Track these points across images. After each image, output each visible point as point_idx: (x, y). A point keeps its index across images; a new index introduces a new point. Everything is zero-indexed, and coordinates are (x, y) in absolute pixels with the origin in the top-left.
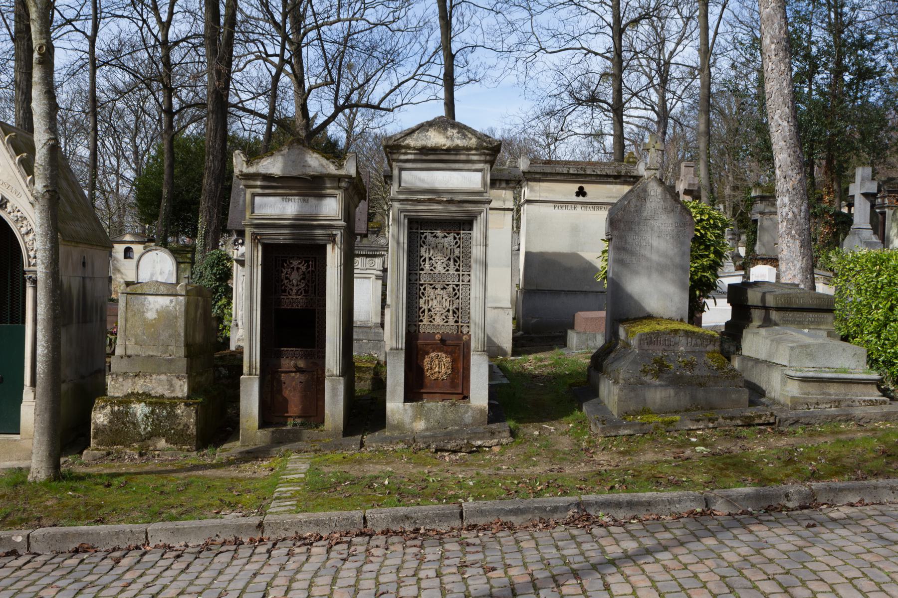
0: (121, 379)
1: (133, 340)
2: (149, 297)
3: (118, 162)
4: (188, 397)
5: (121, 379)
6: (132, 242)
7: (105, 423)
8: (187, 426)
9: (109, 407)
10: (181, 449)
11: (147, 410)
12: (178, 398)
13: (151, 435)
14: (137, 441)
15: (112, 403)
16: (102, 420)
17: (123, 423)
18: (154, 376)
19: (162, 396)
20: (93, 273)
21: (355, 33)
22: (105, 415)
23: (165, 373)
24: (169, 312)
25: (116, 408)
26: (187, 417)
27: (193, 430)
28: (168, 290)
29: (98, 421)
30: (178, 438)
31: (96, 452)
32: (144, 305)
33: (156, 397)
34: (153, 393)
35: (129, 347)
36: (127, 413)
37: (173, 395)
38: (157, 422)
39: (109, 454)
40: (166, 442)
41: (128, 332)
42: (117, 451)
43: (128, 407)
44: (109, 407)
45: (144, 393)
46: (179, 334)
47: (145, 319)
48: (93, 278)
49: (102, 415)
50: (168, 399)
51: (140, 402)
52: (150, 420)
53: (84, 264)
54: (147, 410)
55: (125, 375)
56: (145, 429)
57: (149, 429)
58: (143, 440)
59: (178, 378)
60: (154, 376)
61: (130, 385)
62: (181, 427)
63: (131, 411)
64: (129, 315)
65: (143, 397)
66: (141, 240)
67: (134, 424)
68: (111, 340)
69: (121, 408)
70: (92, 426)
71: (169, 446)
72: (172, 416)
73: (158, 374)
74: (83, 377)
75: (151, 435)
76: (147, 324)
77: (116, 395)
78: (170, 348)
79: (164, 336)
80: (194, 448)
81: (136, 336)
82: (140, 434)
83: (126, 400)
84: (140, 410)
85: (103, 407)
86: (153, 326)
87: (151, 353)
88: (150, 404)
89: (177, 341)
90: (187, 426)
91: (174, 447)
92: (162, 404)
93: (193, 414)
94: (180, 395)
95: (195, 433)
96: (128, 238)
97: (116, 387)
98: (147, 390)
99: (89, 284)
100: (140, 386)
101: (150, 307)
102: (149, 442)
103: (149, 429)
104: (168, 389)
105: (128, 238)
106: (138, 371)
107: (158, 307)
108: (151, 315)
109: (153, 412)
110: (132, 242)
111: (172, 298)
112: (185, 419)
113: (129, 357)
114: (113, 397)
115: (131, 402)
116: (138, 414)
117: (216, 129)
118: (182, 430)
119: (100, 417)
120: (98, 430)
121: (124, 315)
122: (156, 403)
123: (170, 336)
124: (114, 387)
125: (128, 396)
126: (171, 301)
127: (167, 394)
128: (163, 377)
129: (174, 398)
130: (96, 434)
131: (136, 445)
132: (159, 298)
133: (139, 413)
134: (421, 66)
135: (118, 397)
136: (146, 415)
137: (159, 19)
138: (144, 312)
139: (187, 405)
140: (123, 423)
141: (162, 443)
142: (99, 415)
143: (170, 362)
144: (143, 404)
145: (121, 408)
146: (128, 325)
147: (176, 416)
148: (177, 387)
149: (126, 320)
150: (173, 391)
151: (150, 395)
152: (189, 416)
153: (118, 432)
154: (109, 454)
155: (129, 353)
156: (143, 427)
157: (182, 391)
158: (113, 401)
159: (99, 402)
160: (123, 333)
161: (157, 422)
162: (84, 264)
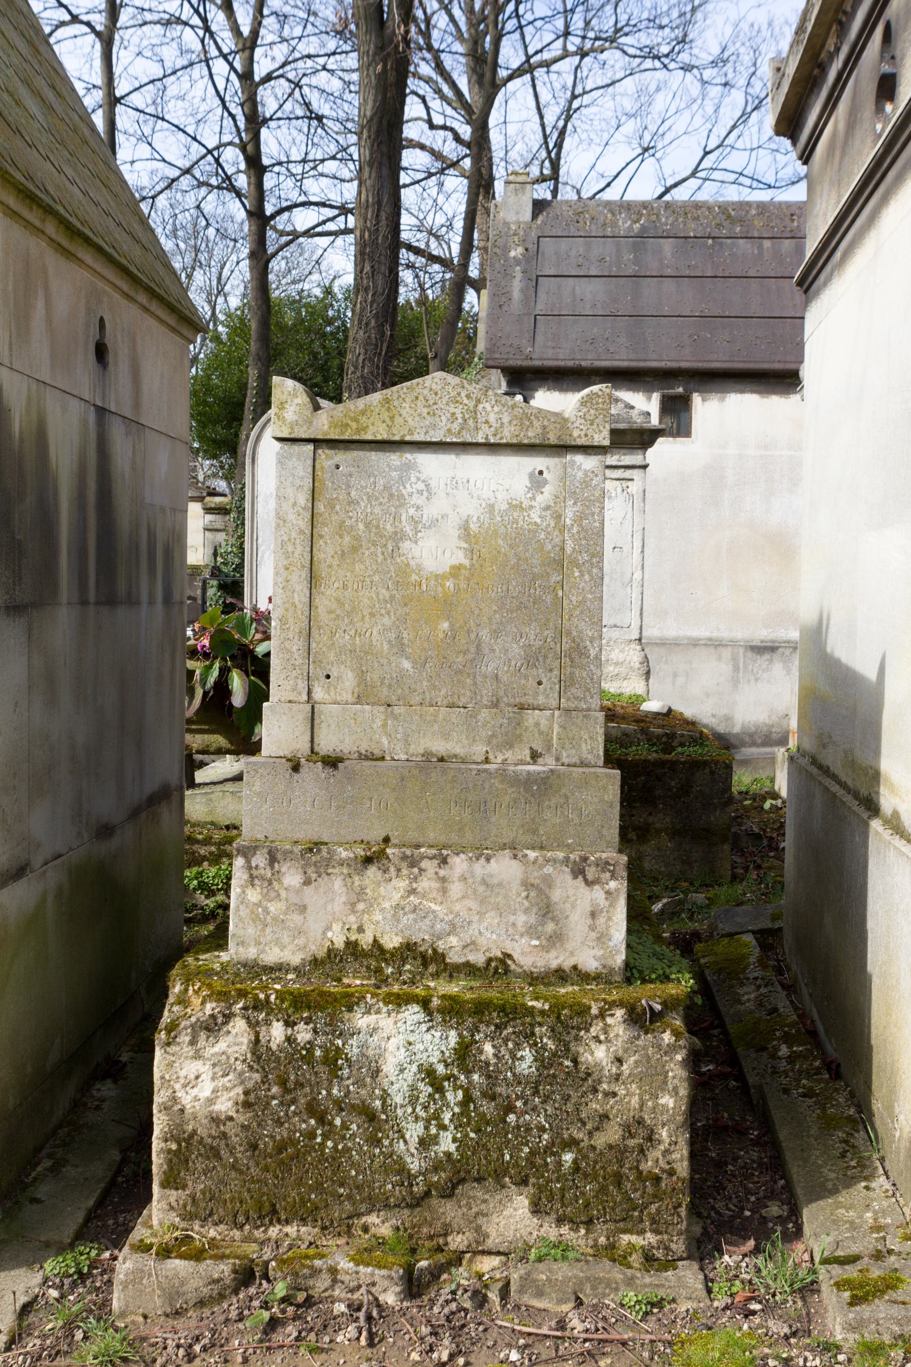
0: (292, 877)
1: (348, 680)
4: (632, 972)
5: (292, 877)
7: (224, 1106)
8: (641, 1130)
9: (239, 1025)
10: (611, 1252)
11: (437, 1044)
12: (580, 976)
13: (456, 1177)
14: (385, 1205)
15: (257, 1006)
16: (205, 1090)
17: (313, 1110)
18: (459, 864)
19: (499, 968)
20: (137, 404)
21: (585, 93)
22: (222, 1066)
23: (514, 848)
25: (277, 1032)
26: (639, 1077)
27: (671, 1152)
29: (186, 1099)
30: (596, 1194)
31: (176, 1264)
33: (469, 969)
34: (454, 948)
35: (328, 713)
36: (333, 1060)
37: (555, 959)
38: (487, 1108)
39: (247, 1275)
40: (536, 1209)
41: (320, 641)
42: (296, 1265)
43: (335, 1028)
44: (239, 1025)
45: (409, 949)
47: (405, 570)
48: (135, 425)
49: (202, 1068)
50: (533, 979)
51: (399, 1001)
52: (454, 1097)
53: (101, 352)
54: (437, 1044)
55: (313, 854)
56: (425, 1143)
57: (447, 1144)
58: (418, 1202)
59: (578, 871)
60: (459, 864)
61: (339, 904)
62: (612, 1134)
63: (353, 1048)
64: (327, 551)
65: (405, 969)
67: (371, 1116)
69: (303, 1034)
70: (160, 1124)
71: (551, 1231)
72: (561, 1075)
73: (481, 851)
74: (105, 831)
75: (456, 1177)
77: (272, 956)
78: (532, 717)
80: (679, 1246)
81: (361, 657)
82: (402, 1170)
83: (325, 989)
84: (398, 1043)
85: (212, 1028)
86: (447, 606)
87: (440, 747)
88: (451, 1011)
90: (641, 1130)
91: (577, 1238)
92: (511, 1012)
93: (676, 1071)
94: (590, 962)
95: (683, 1168)
97: (275, 921)
98: (421, 934)
99: (121, 446)
100: (388, 911)
101: (431, 511)
102: (449, 1211)
103: (447, 1144)
104: (531, 931)
106: (375, 834)
107: (471, 509)
108: (435, 553)
109: (464, 1054)
111: (538, 462)
112: (631, 1097)
113: (332, 762)
114: (256, 969)
115: (350, 1001)
116: (389, 1067)
117: (379, 203)
118: (618, 1151)
119: (197, 1078)
120: (186, 1146)
122: (480, 1009)
123: (532, 659)
124: (260, 919)
125: (331, 961)
126: (537, 480)
127: (528, 955)
128: (504, 868)
129: (561, 976)
130: (179, 1162)
131: (381, 1225)
132: (476, 466)
133: (393, 1059)
134: (706, 153)
135: (280, 968)
136: (429, 1073)
137: (236, 29)
138: (398, 537)
139: (642, 1020)
140: (313, 1110)
141: (513, 1216)
142: (191, 1068)
143: (539, 788)
144: (413, 1013)
145: (303, 1034)
146: (323, 603)
147: (585, 1079)
148: (577, 923)
150: (555, 940)
151: (439, 957)
152: (653, 1080)
153: (287, 1155)
154: (247, 1275)
155: (327, 743)
156: (414, 1131)
157: (602, 938)
158: (248, 991)
159: (186, 1000)
160: (297, 646)
161: (487, 1108)
162: (101, 352)
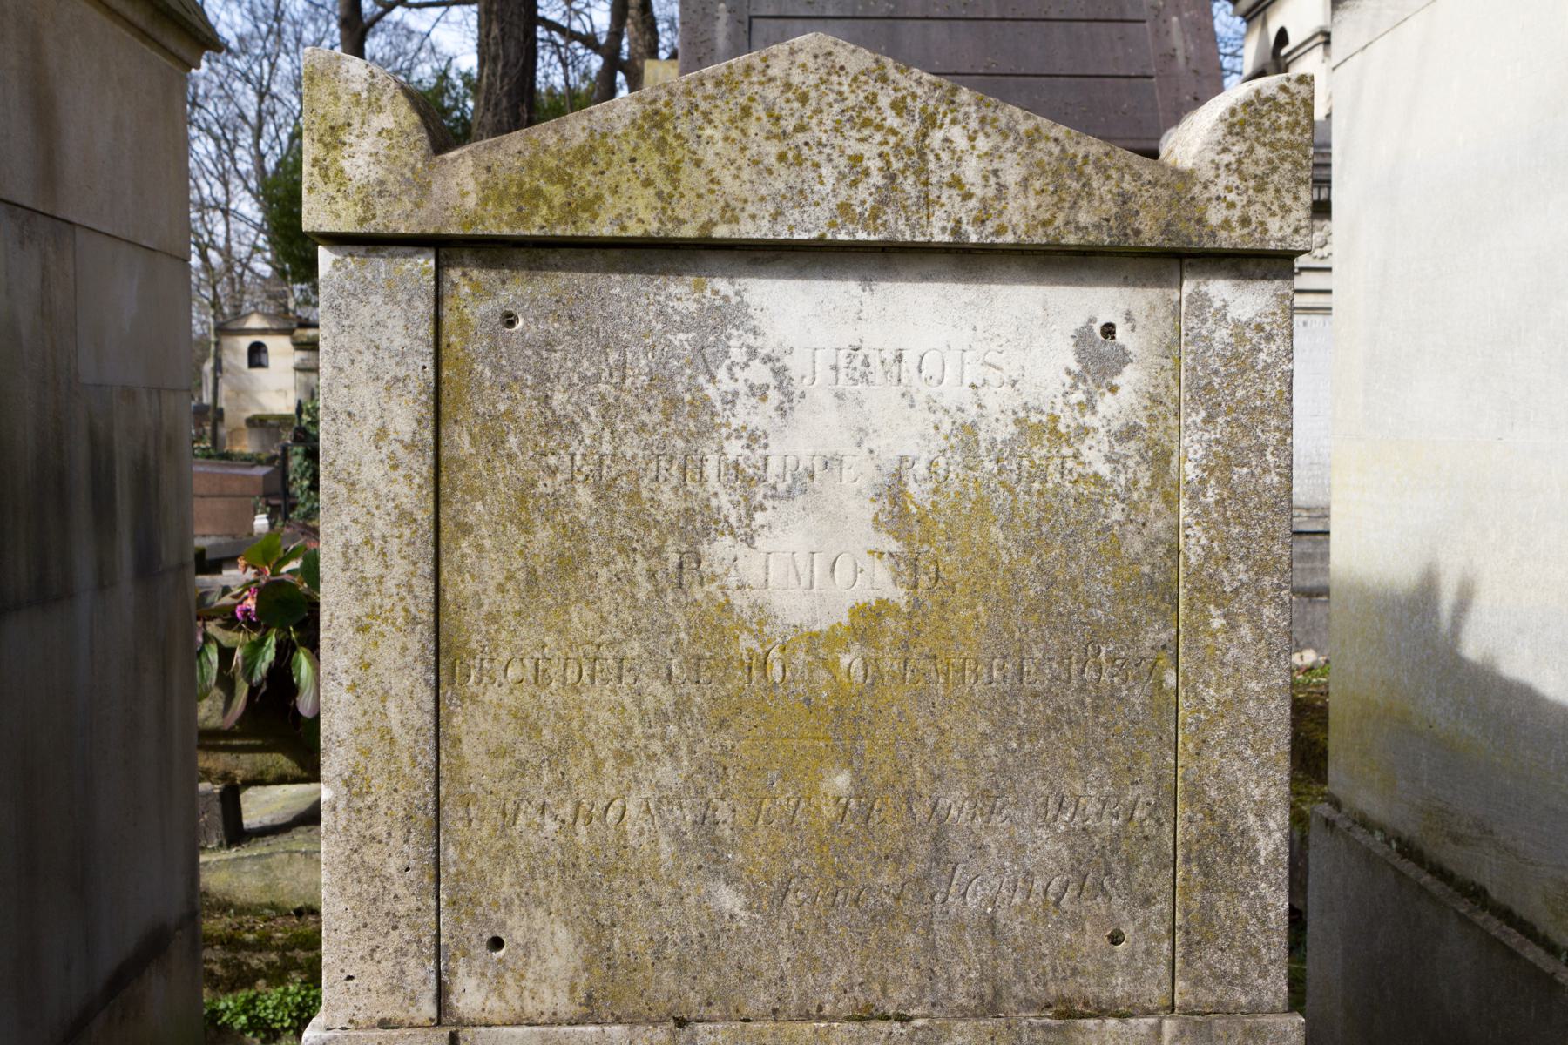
1: (557, 952)
2: (785, 308)
3: (227, 193)
6: (264, 332)
24: (1062, 520)
28: (1064, 178)
32: (702, 418)
41: (469, 840)
46: (1223, 840)
47: (717, 622)
64: (484, 572)
66: (284, 326)
68: (226, 654)
76: (730, 683)
79: (1011, 862)
81: (594, 881)
86: (844, 723)
89: (1192, 936)
96: (255, 322)
101: (791, 447)
105: (255, 322)
107: (909, 438)
108: (806, 570)
110: (264, 332)
111: (1102, 301)
121: (402, 572)
123: (1094, 867)
126: (1099, 352)
138: (698, 524)
146: (475, 730)
149: (443, 656)
